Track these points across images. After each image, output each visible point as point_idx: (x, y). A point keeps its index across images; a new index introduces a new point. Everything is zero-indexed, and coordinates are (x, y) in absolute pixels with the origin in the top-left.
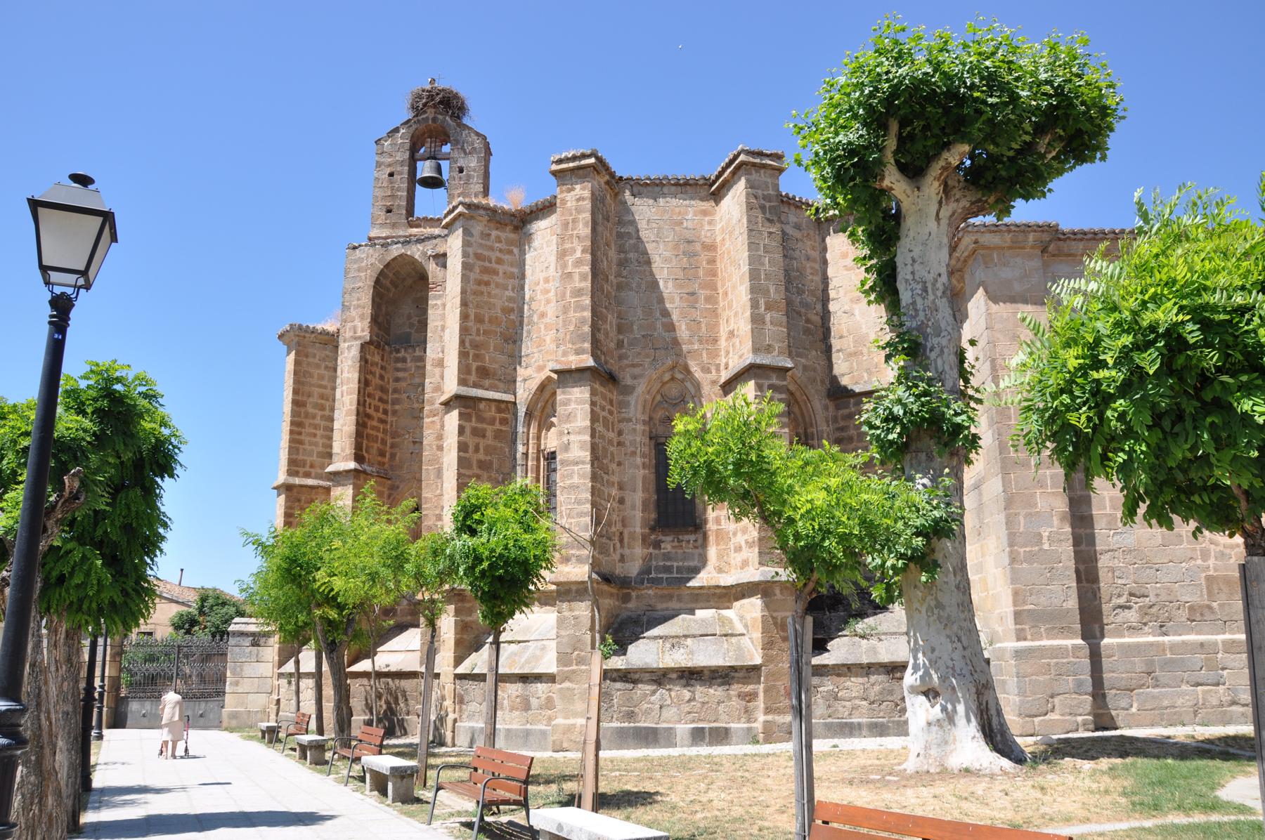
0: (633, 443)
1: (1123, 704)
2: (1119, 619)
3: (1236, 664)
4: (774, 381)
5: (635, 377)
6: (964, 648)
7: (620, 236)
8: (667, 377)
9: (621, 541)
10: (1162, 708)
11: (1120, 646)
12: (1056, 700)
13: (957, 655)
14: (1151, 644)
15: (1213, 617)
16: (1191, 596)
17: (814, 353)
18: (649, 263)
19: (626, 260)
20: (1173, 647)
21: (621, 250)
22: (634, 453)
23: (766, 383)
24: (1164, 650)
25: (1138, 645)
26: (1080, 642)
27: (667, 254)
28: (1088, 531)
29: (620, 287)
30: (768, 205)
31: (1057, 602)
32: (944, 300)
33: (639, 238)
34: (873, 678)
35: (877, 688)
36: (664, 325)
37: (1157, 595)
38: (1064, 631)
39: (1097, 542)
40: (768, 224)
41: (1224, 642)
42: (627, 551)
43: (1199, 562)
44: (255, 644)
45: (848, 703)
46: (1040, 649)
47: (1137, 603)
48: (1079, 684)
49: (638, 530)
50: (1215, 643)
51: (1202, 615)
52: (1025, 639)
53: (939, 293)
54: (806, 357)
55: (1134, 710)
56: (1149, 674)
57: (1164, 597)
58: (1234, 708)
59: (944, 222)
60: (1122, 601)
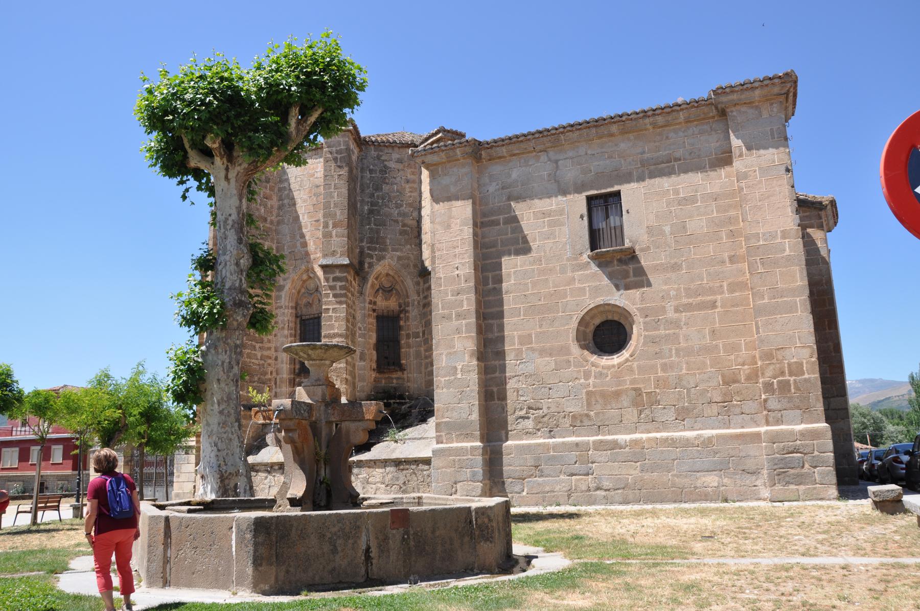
0: (283, 321)
1: (517, 489)
2: (520, 426)
3: (602, 459)
4: (338, 274)
5: (285, 280)
6: (219, 450)
7: (280, 190)
8: (305, 277)
9: (276, 384)
10: (544, 492)
11: (517, 446)
12: (458, 485)
13: (213, 455)
14: (539, 445)
15: (590, 423)
16: (574, 407)
17: (409, 246)
18: (295, 204)
19: (283, 205)
20: (555, 447)
21: (280, 199)
22: (283, 328)
23: (331, 276)
24: (548, 449)
25: (529, 446)
26: (479, 444)
27: (305, 197)
28: (501, 362)
29: (279, 223)
30: (339, 156)
31: (464, 416)
32: (233, 230)
33: (290, 189)
34: (388, 469)
35: (390, 476)
36: (301, 244)
37: (549, 408)
38: (468, 437)
39: (507, 370)
40: (338, 169)
41: (594, 442)
42: (278, 390)
43: (582, 381)
44: (187, 453)
45: (374, 486)
46: (449, 449)
47: (533, 414)
48: (474, 474)
49: (285, 376)
50: (588, 443)
51: (581, 421)
52: (442, 443)
53: (229, 227)
54: (401, 250)
55: (524, 493)
56: (537, 467)
57: (552, 410)
58: (598, 492)
59: (233, 181)
60: (523, 413)
